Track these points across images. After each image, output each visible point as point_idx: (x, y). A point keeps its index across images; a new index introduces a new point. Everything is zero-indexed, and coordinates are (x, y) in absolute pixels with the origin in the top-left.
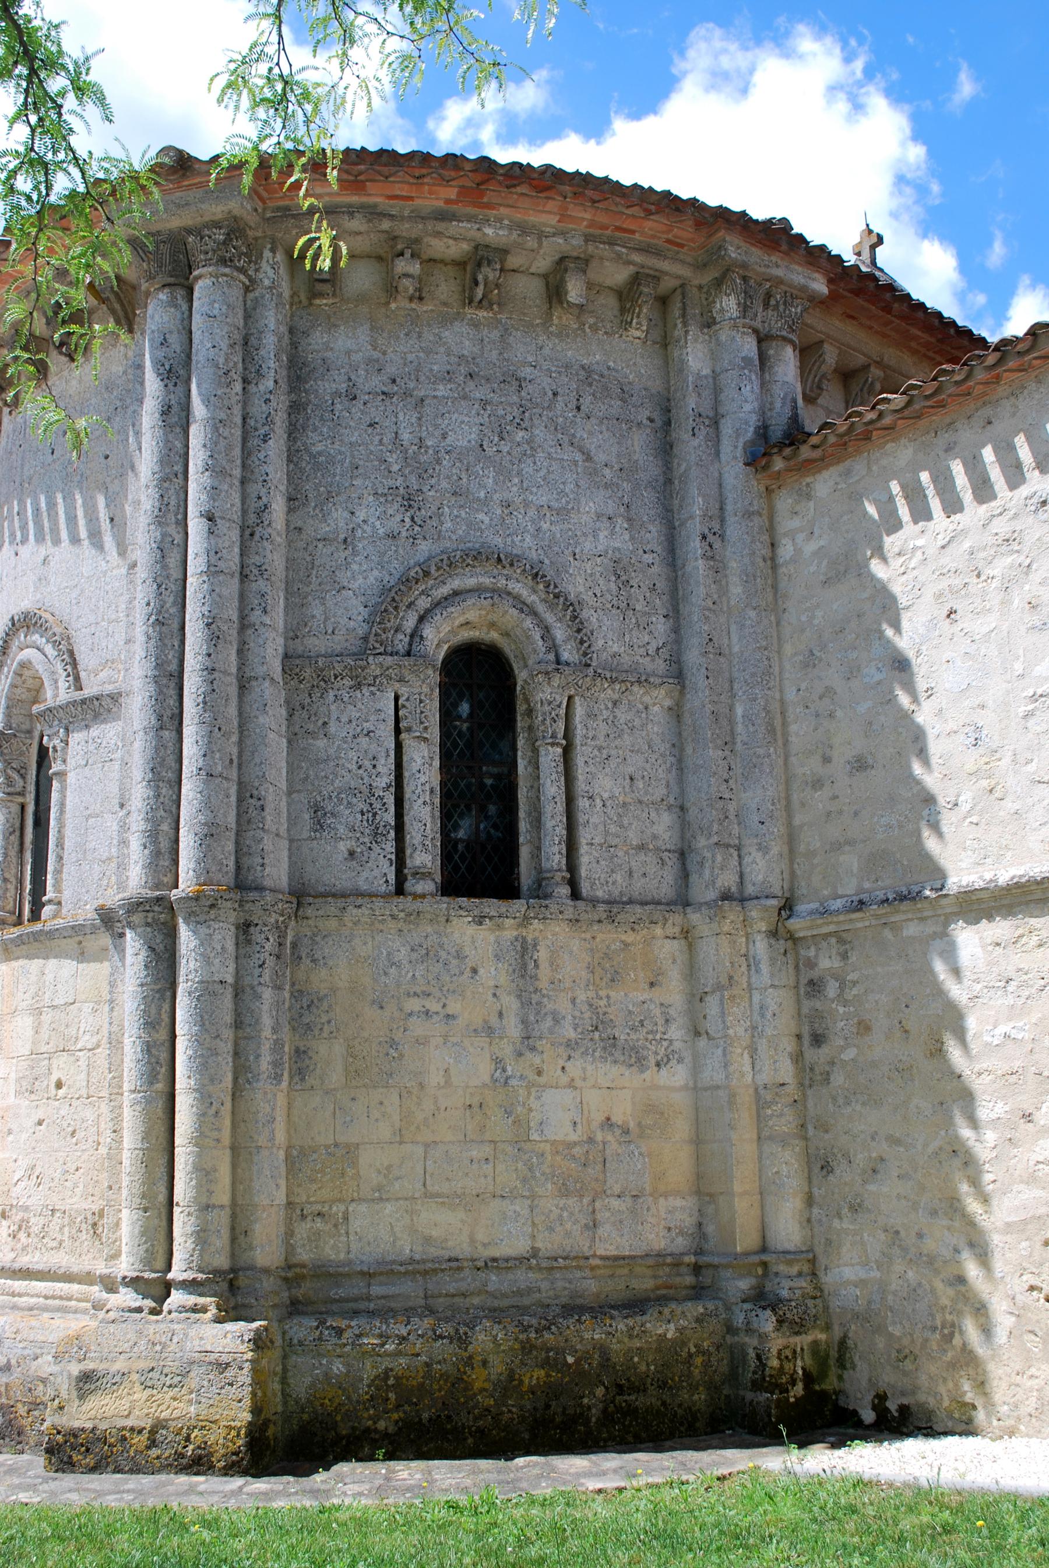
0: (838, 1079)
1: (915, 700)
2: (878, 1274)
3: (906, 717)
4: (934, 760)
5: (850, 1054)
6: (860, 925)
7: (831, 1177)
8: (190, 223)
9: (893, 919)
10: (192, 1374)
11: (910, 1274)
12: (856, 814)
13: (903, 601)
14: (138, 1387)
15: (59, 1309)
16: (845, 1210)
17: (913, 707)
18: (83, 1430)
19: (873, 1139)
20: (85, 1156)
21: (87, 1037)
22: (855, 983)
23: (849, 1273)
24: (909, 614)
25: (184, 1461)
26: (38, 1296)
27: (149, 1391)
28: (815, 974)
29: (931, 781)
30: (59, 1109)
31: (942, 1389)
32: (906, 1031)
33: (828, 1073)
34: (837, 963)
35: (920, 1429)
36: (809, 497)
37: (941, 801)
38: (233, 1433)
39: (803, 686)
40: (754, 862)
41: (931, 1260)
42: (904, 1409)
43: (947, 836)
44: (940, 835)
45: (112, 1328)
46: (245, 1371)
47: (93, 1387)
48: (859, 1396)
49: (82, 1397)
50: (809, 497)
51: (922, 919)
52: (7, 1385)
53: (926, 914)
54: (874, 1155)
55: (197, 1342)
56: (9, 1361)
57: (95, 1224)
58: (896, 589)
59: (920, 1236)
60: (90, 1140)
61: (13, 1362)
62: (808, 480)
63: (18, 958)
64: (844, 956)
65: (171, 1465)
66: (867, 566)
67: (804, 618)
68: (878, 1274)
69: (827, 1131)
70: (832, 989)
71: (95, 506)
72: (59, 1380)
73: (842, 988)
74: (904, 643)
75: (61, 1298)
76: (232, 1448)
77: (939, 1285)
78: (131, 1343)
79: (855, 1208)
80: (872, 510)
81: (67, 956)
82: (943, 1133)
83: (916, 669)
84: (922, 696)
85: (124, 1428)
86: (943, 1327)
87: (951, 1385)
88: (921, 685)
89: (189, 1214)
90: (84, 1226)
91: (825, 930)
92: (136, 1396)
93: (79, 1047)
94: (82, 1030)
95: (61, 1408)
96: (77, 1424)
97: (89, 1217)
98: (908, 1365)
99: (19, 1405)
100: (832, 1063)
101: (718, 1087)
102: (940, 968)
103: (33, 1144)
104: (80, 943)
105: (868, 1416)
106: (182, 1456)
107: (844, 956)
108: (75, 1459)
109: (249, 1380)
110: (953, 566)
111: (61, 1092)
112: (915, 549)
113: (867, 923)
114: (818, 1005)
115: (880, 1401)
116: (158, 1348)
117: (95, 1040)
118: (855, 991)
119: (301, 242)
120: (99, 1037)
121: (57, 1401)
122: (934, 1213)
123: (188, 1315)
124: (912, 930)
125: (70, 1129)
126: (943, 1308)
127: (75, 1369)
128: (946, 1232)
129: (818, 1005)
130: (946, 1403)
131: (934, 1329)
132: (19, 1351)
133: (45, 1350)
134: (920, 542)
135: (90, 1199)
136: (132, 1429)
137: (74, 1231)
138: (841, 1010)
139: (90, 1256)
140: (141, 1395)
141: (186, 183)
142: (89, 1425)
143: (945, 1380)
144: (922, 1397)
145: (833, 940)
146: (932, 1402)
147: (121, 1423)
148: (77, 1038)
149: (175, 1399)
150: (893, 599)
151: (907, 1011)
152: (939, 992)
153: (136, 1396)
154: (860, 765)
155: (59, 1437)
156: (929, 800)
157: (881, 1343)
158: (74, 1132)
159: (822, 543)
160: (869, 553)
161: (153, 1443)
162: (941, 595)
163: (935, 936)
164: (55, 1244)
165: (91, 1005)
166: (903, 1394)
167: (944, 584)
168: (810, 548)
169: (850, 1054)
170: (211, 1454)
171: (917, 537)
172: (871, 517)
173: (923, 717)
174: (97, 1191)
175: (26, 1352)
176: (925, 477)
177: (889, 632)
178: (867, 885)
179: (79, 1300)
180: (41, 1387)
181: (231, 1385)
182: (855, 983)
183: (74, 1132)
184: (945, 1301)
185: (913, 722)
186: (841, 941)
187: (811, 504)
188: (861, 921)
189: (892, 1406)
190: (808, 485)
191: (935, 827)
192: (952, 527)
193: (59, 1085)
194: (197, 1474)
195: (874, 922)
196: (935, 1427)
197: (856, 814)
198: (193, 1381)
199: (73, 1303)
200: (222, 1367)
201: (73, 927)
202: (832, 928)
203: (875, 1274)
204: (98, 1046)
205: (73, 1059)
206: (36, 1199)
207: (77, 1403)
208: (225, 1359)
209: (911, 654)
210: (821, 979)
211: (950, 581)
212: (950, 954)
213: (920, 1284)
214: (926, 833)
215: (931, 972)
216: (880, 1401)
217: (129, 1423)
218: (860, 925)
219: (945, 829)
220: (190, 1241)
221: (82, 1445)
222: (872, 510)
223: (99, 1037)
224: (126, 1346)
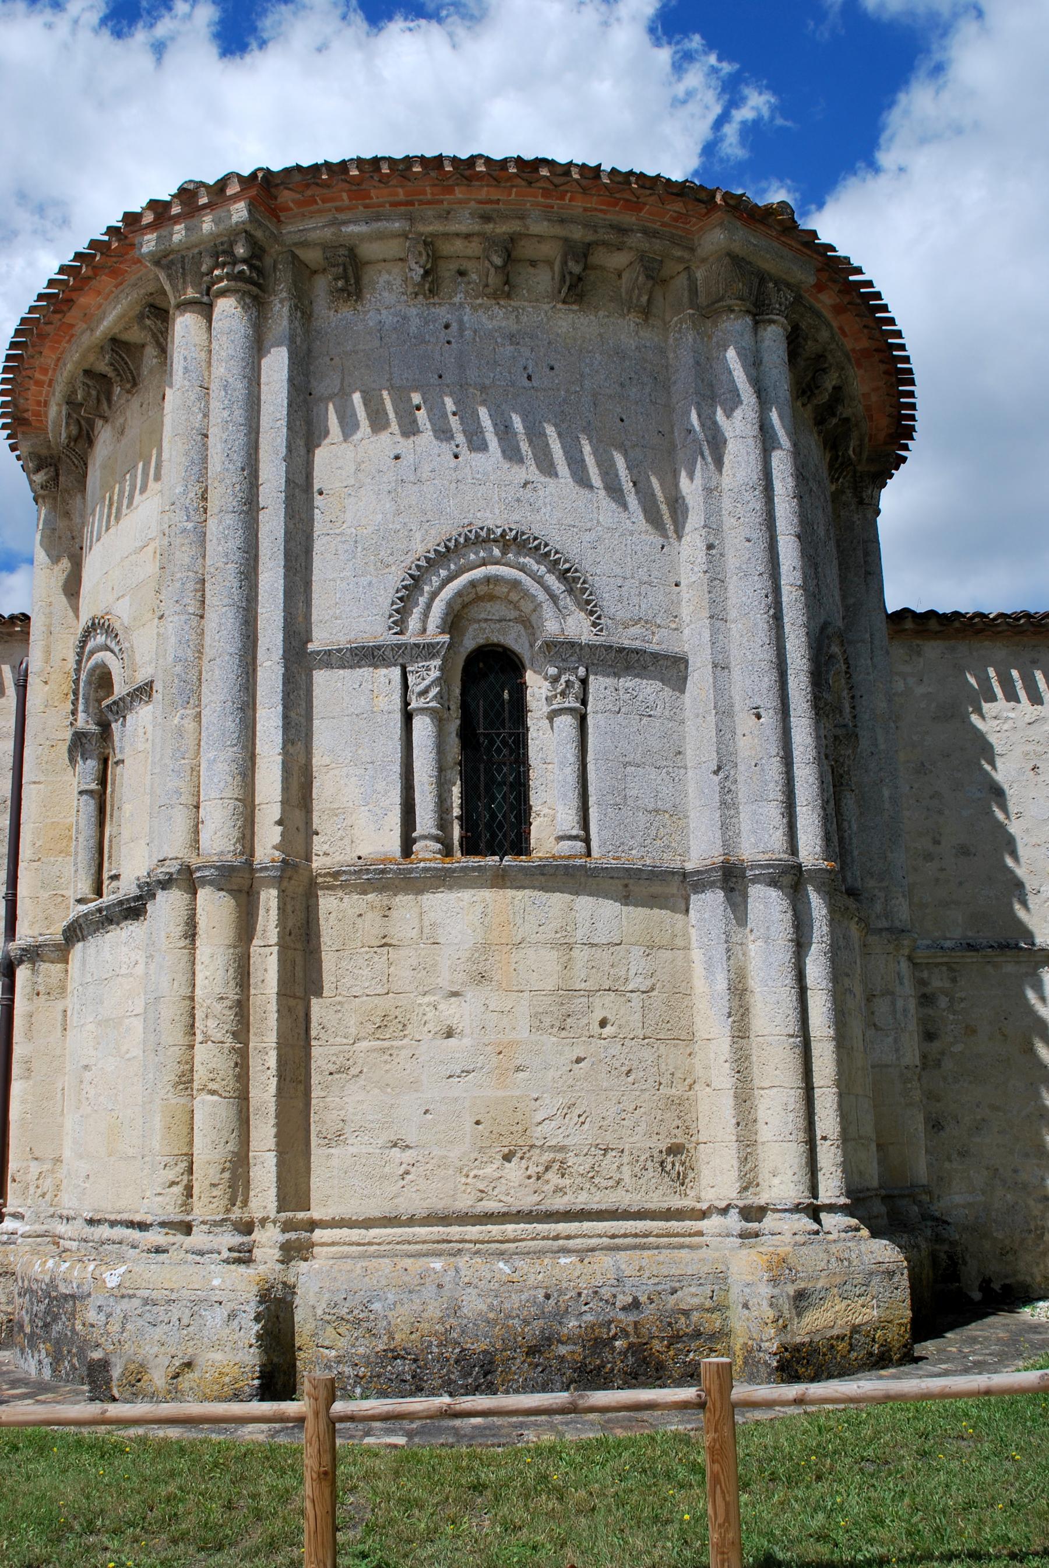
0: (948, 1064)
1: (1008, 817)
2: (983, 1198)
3: (1001, 827)
4: (1022, 860)
5: (958, 1048)
6: (969, 960)
7: (942, 1133)
8: (773, 271)
9: (996, 960)
10: (872, 1284)
11: (1009, 1196)
12: (960, 883)
13: (998, 749)
14: (837, 1300)
15: (635, 1247)
16: (955, 1156)
17: (1006, 822)
18: (803, 1344)
19: (978, 1106)
20: (646, 1095)
21: (640, 979)
22: (962, 1000)
23: (958, 1199)
24: (1003, 760)
25: (873, 1359)
26: (600, 1236)
27: (846, 1302)
28: (928, 990)
29: (1021, 872)
30: (606, 1049)
31: (1035, 1270)
32: (1004, 1035)
33: (939, 1060)
34: (947, 984)
35: (1018, 1299)
36: (919, 654)
37: (1028, 887)
38: (903, 1329)
39: (916, 786)
40: (900, 905)
41: (1025, 1186)
42: (1007, 1288)
43: (1033, 911)
44: (1027, 908)
45: (804, 1250)
46: (905, 1276)
47: (806, 1304)
48: (969, 1282)
49: (799, 1315)
50: (919, 654)
51: (1017, 963)
52: (636, 1323)
53: (1022, 959)
54: (979, 1117)
55: (870, 1256)
56: (635, 1299)
57: (662, 1163)
58: (992, 739)
59: (1015, 1171)
60: (651, 1080)
61: (643, 1299)
62: (918, 642)
63: (525, 888)
64: (954, 980)
65: (864, 1364)
66: (969, 718)
67: (915, 738)
68: (983, 1198)
69: (939, 1101)
70: (943, 1002)
71: (613, 465)
72: (781, 1301)
73: (952, 1000)
74: (999, 777)
75: (636, 1235)
76: (903, 1341)
77: (1031, 1203)
78: (825, 1261)
79: (963, 1154)
80: (972, 681)
81: (607, 896)
82: (1033, 1103)
83: (1008, 798)
84: (1013, 817)
85: (832, 1337)
86: (1036, 1229)
87: (1042, 1266)
88: (1012, 808)
89: (838, 1147)
90: (649, 1164)
91: (939, 960)
92: (837, 1308)
93: (630, 988)
94: (632, 972)
95: (785, 1327)
96: (798, 1340)
97: (656, 1154)
98: (1010, 1257)
99: (655, 1342)
100: (943, 1053)
101: (887, 1066)
102: (1031, 995)
103: (570, 1082)
104: (626, 886)
105: (977, 1296)
106: (871, 1354)
107: (954, 980)
108: (800, 1372)
109: (907, 1284)
110: (1037, 738)
111: (608, 1030)
112: (1007, 718)
113: (975, 960)
114: (931, 1012)
115: (985, 1284)
116: (846, 1263)
117: (649, 983)
118: (962, 1005)
119: (775, 317)
120: (653, 980)
121: (781, 1321)
122: (1027, 1155)
123: (853, 1233)
124: (1009, 968)
125: (625, 1069)
126: (1035, 1218)
127: (791, 1289)
128: (1035, 1168)
129: (931, 1012)
130: (1039, 1279)
131: (1030, 1231)
132: (652, 1288)
133: (685, 1283)
134: (1012, 715)
135: (655, 1137)
136: (838, 1337)
137: (637, 1169)
138: (951, 1017)
139: (660, 1192)
140: (841, 1306)
141: (783, 239)
142: (807, 1339)
143: (1038, 1264)
144: (1020, 1278)
145: (944, 968)
146: (1028, 1279)
147: (830, 1333)
148: (627, 979)
149: (863, 1306)
150: (991, 747)
151: (1006, 1022)
152: (1030, 1011)
153: (837, 1308)
154: (964, 851)
155: (787, 1354)
156: (1019, 885)
157: (987, 1245)
158: (629, 1071)
159: (930, 690)
160: (971, 709)
161: (852, 1348)
162: (1028, 754)
163: (1027, 974)
164: (611, 1183)
165: (643, 949)
166: (1006, 1277)
167: (1029, 747)
168: (920, 690)
169: (958, 1048)
170: (890, 1350)
171: (1008, 711)
172: (971, 685)
173: (1014, 828)
174: (663, 1130)
175: (659, 1288)
176: (1015, 673)
177: (988, 767)
178: (970, 934)
179: (657, 1236)
180: (683, 1319)
181: (897, 1289)
182: (962, 1000)
183: (629, 1071)
184: (1036, 1213)
185: (1007, 832)
186: (951, 969)
187: (921, 660)
188: (970, 957)
189: (996, 1286)
190: (918, 646)
191: (1024, 904)
192: (1036, 713)
193: (603, 1023)
194: (883, 1368)
195: (980, 960)
196: (1032, 1296)
197: (960, 883)
198: (874, 1289)
199: (651, 1239)
200: (891, 1274)
201: (627, 870)
202: (945, 960)
203: (981, 1198)
204: (652, 989)
205: (623, 999)
206: (579, 1138)
207: (796, 1320)
208: (892, 1267)
209: (1006, 787)
210: (933, 994)
211: (1034, 748)
212: (1038, 987)
213: (1017, 1203)
214: (1017, 906)
215: (1026, 999)
216: (985, 1284)
217: (835, 1332)
218: (969, 960)
219: (1031, 906)
220: (839, 1170)
221: (804, 1358)
222: (972, 681)
223: (653, 980)
224: (823, 1264)
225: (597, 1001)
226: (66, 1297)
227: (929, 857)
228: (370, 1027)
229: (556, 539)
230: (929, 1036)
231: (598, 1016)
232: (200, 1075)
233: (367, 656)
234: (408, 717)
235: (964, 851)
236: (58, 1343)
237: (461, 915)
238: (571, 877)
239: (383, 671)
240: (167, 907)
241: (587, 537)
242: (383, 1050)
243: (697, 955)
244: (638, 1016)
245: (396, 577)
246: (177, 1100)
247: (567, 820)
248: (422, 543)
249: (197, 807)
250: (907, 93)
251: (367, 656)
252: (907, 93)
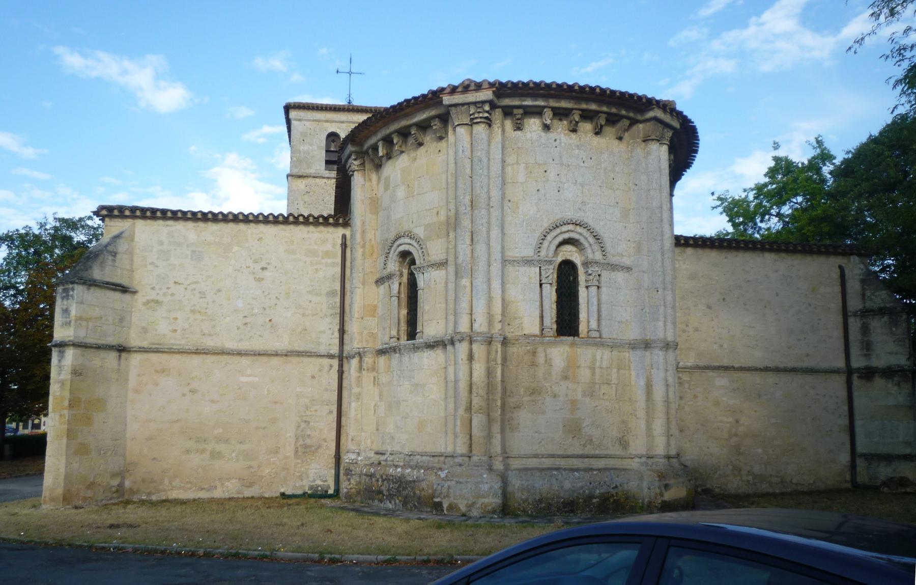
5: (691, 403)
70: (686, 386)
154: (697, 330)
169: (691, 403)
225: (602, 387)
226: (410, 482)
227: (684, 331)
228: (528, 393)
229: (591, 223)
230: (681, 398)
231: (603, 391)
232: (474, 408)
233: (528, 262)
234: (541, 285)
235: (697, 330)
236: (406, 497)
237: (559, 353)
238: (599, 342)
239: (533, 269)
240: (462, 349)
241: (602, 223)
242: (533, 401)
243: (633, 373)
244: (614, 393)
245: (537, 235)
246: (467, 415)
247: (594, 324)
248: (546, 224)
249: (471, 314)
250: (871, 136)
251: (528, 262)
252: (871, 136)
